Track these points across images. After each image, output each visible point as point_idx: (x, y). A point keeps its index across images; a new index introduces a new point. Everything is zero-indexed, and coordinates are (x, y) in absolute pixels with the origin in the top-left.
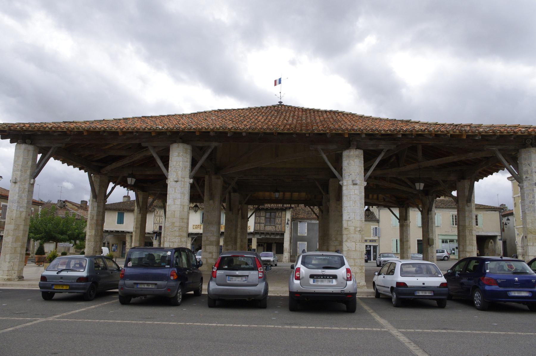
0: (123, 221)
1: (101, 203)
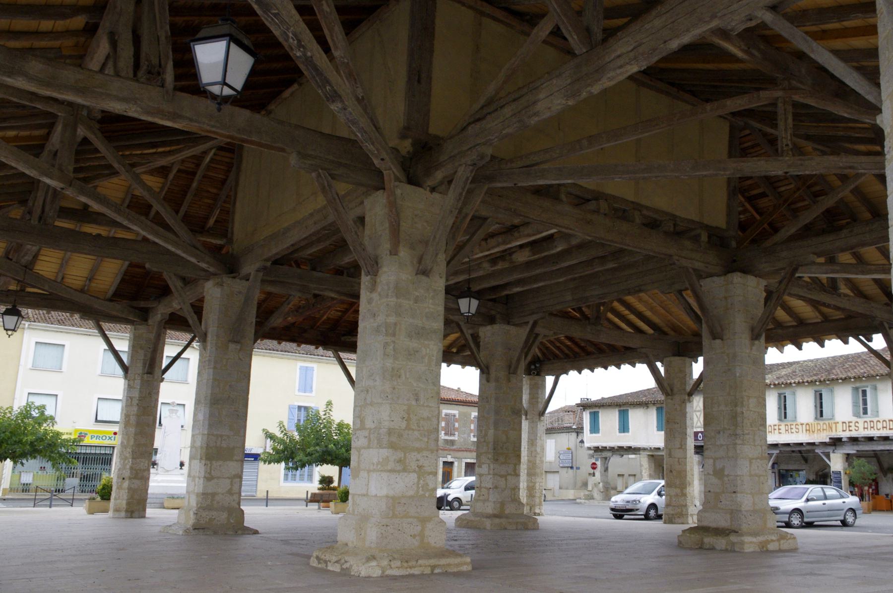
0: (628, 426)
1: (136, 381)
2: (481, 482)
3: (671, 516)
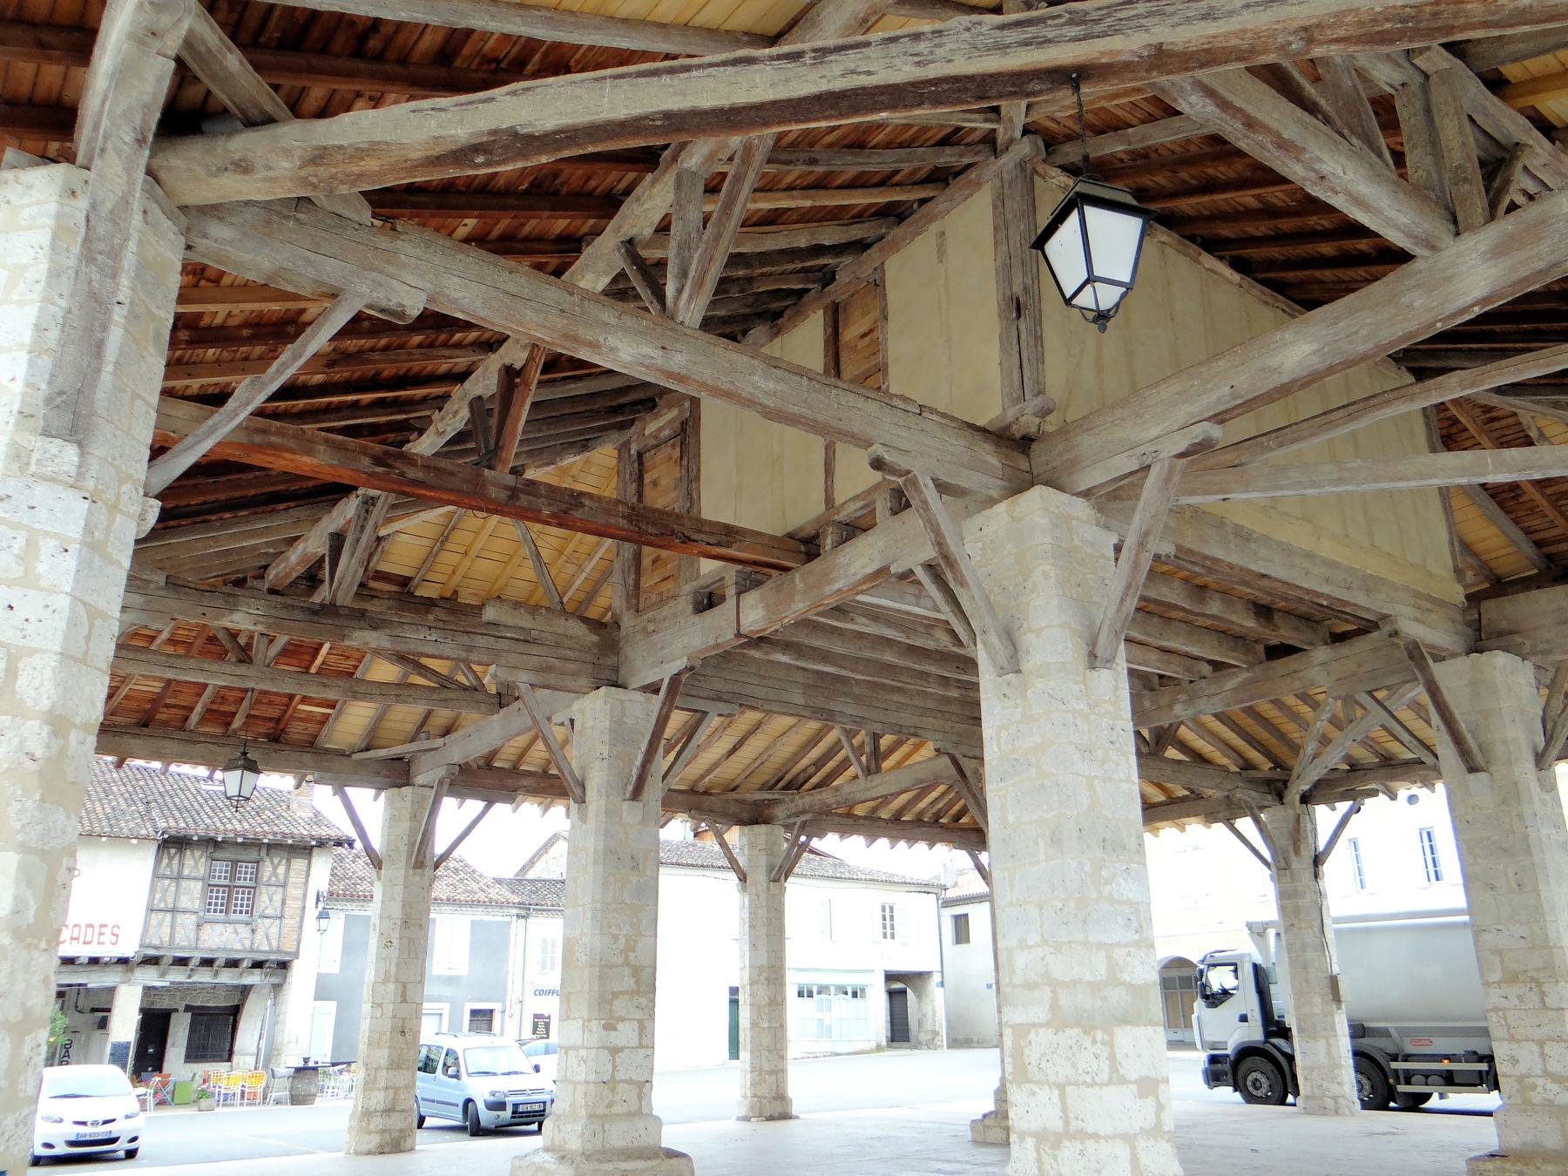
2: (614, 1068)
3: (396, 1134)
